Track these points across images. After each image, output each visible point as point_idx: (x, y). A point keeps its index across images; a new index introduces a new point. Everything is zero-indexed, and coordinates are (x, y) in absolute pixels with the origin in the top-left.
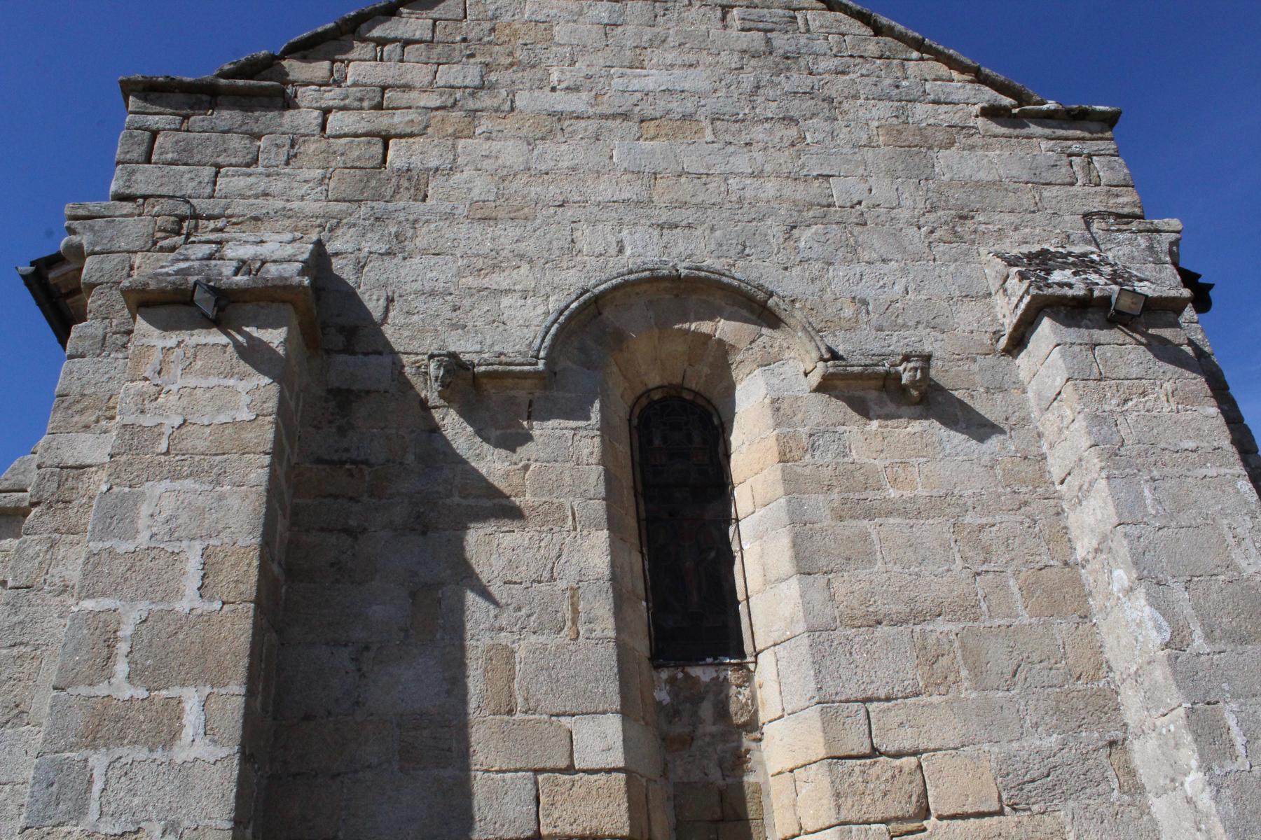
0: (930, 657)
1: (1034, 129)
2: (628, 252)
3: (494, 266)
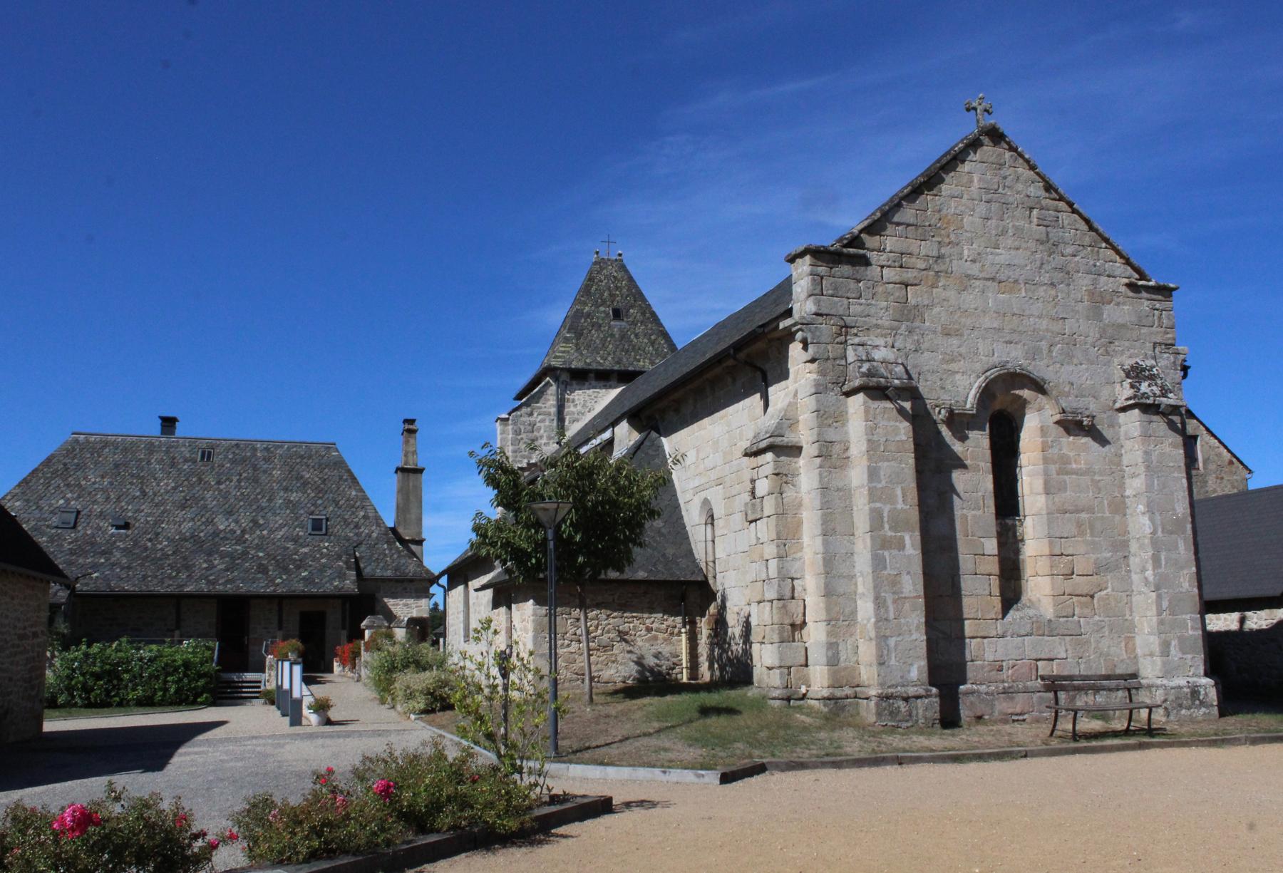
0: (1079, 525)
1: (1144, 294)
2: (996, 355)
3: (953, 360)
